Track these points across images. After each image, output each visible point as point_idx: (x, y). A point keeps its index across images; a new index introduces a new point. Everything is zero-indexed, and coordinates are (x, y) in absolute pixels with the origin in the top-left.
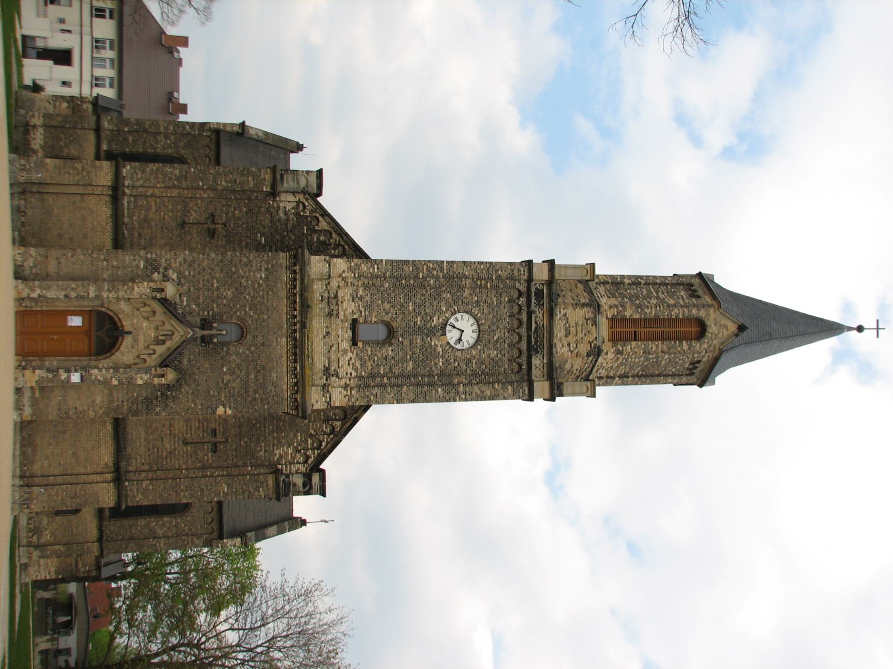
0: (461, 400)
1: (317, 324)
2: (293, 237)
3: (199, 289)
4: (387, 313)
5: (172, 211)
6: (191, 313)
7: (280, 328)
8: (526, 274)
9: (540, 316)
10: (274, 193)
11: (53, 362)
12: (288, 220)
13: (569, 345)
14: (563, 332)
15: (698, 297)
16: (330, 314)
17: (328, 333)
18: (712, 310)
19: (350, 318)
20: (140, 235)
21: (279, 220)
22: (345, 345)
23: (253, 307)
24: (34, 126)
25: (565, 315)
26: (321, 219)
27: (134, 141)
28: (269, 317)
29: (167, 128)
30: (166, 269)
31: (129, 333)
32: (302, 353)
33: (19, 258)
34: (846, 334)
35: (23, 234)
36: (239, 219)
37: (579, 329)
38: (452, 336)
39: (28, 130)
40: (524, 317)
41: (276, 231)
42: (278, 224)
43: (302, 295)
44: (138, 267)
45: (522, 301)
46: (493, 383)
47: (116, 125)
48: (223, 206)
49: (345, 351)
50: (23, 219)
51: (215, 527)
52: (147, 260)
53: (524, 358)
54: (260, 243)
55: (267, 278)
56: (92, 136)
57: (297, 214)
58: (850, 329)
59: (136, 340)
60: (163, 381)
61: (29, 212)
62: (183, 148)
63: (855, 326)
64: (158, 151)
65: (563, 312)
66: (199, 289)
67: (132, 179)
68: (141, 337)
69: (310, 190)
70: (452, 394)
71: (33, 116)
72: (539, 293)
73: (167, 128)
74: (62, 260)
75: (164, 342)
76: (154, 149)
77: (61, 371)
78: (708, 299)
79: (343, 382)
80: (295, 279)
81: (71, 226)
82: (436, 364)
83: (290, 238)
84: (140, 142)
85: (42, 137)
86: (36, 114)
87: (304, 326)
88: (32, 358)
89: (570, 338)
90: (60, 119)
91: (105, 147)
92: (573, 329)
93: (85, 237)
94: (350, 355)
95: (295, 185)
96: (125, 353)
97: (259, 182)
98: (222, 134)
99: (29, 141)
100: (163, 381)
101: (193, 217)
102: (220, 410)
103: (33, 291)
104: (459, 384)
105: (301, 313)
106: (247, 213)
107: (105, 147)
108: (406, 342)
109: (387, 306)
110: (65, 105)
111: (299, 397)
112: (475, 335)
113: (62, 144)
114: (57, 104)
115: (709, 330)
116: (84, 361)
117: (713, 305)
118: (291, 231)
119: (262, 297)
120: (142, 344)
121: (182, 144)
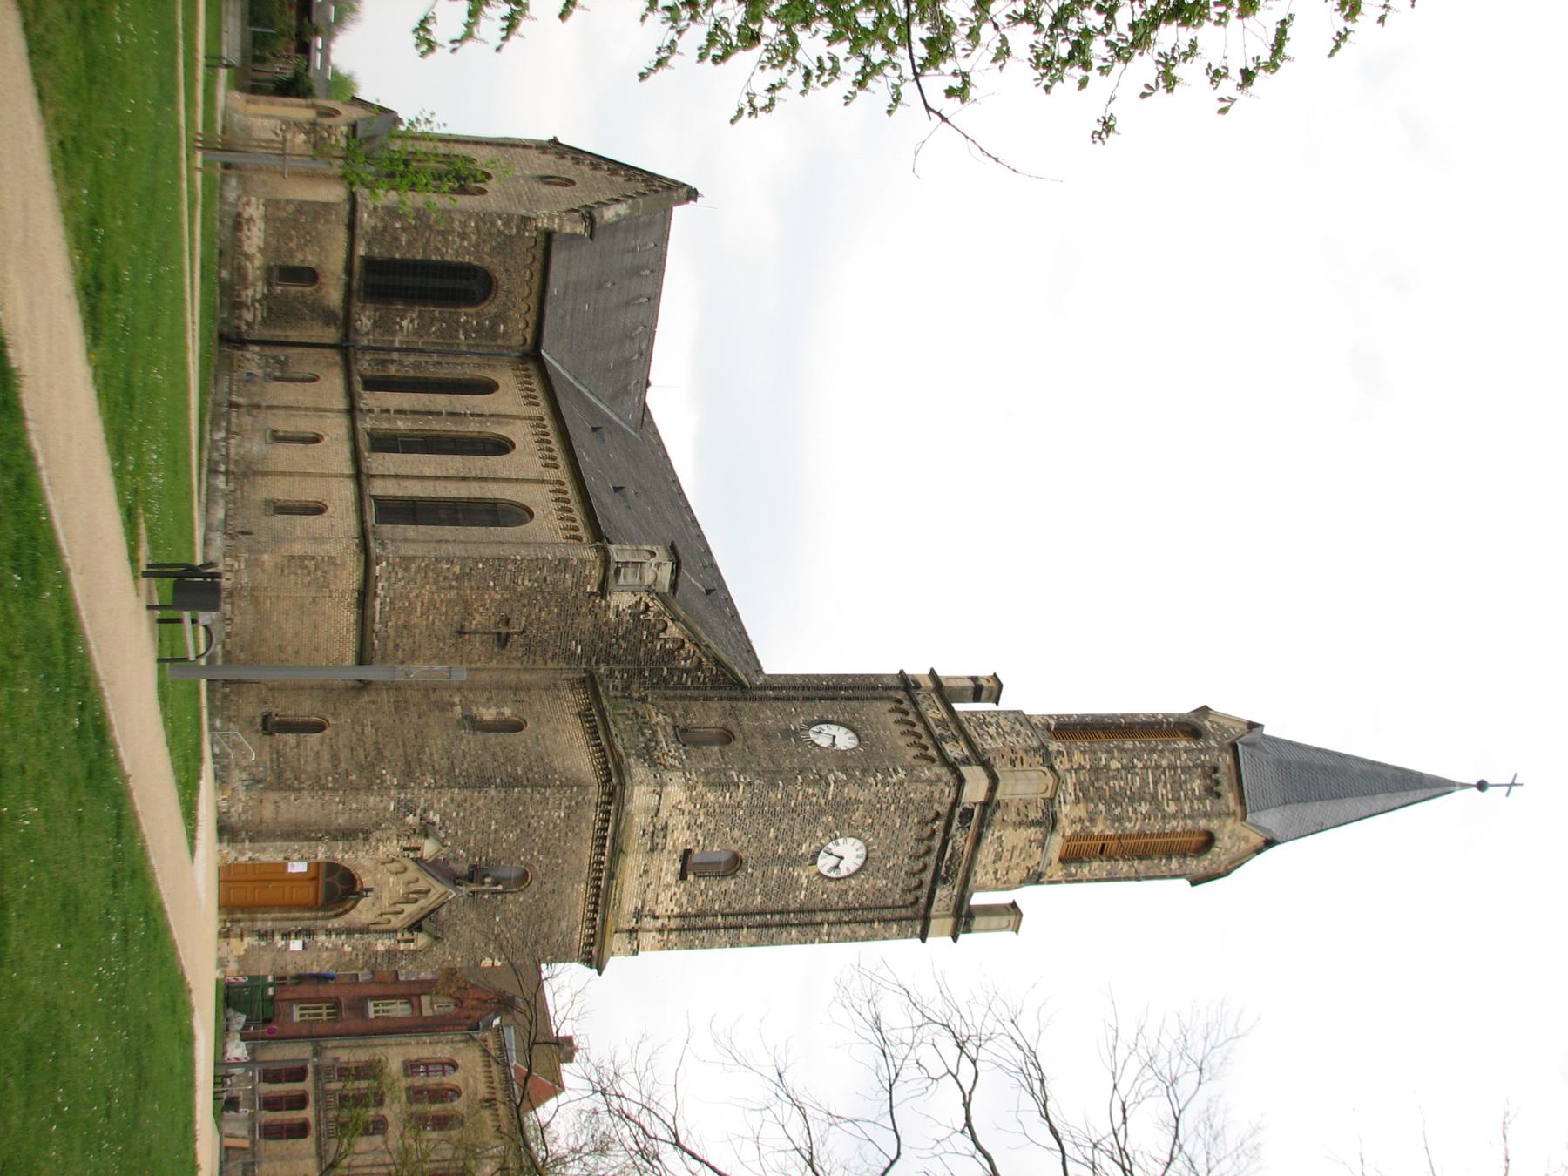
0: (821, 941)
1: (632, 864)
2: (624, 645)
3: (470, 833)
4: (736, 842)
5: (446, 614)
6: (455, 860)
7: (580, 872)
8: (953, 795)
9: (961, 840)
10: (603, 591)
11: (265, 922)
12: (620, 623)
13: (996, 872)
14: (991, 857)
15: (1218, 795)
16: (652, 850)
17: (646, 872)
18: (1230, 821)
19: (681, 849)
20: (396, 646)
21: (607, 623)
22: (671, 879)
23: (545, 850)
24: (251, 219)
25: (1000, 837)
26: (670, 623)
27: (409, 242)
28: (565, 861)
29: (465, 225)
30: (425, 811)
31: (370, 890)
32: (606, 904)
33: (225, 804)
34: (1457, 796)
35: (228, 647)
36: (546, 622)
37: (1017, 853)
38: (825, 863)
39: (240, 223)
40: (937, 843)
41: (601, 637)
42: (605, 629)
43: (614, 840)
44: (386, 809)
45: (939, 824)
46: (872, 921)
47: (382, 219)
48: (524, 606)
49: (668, 886)
50: (228, 629)
51: (528, 337)
52: (399, 801)
53: (925, 890)
54: (573, 654)
55: (568, 817)
56: (342, 235)
57: (635, 616)
58: (1465, 786)
59: (379, 898)
60: (412, 946)
61: (238, 619)
62: (490, 255)
63: (1475, 782)
64: (448, 258)
65: (997, 834)
66: (470, 833)
67: (388, 579)
68: (386, 894)
69: (658, 589)
70: (810, 936)
71: (248, 203)
72: (967, 814)
73: (465, 225)
74: (282, 804)
75: (416, 901)
76: (442, 255)
77: (278, 938)
78: (1231, 800)
79: (659, 923)
80: (607, 821)
81: (296, 635)
82: (795, 897)
83: (620, 647)
84: (419, 244)
85: (261, 234)
86: (254, 199)
87: (611, 876)
88: (239, 916)
89: (999, 865)
90: (291, 208)
91: (361, 251)
92: (1006, 854)
93: (316, 649)
94: (674, 889)
95: (637, 581)
96: (363, 912)
97: (581, 580)
98: (556, 236)
99: (240, 241)
100: (412, 946)
101: (477, 621)
102: (487, 962)
103: (242, 853)
104: (822, 924)
105: (611, 860)
106: (558, 615)
107: (361, 251)
108: (757, 874)
109: (737, 833)
110: (302, 137)
111: (594, 950)
112: (860, 861)
113: (293, 245)
114: (289, 136)
115: (1218, 844)
116: (306, 919)
117: (1234, 814)
118: (623, 637)
119: (559, 840)
120: (386, 902)
121: (487, 248)
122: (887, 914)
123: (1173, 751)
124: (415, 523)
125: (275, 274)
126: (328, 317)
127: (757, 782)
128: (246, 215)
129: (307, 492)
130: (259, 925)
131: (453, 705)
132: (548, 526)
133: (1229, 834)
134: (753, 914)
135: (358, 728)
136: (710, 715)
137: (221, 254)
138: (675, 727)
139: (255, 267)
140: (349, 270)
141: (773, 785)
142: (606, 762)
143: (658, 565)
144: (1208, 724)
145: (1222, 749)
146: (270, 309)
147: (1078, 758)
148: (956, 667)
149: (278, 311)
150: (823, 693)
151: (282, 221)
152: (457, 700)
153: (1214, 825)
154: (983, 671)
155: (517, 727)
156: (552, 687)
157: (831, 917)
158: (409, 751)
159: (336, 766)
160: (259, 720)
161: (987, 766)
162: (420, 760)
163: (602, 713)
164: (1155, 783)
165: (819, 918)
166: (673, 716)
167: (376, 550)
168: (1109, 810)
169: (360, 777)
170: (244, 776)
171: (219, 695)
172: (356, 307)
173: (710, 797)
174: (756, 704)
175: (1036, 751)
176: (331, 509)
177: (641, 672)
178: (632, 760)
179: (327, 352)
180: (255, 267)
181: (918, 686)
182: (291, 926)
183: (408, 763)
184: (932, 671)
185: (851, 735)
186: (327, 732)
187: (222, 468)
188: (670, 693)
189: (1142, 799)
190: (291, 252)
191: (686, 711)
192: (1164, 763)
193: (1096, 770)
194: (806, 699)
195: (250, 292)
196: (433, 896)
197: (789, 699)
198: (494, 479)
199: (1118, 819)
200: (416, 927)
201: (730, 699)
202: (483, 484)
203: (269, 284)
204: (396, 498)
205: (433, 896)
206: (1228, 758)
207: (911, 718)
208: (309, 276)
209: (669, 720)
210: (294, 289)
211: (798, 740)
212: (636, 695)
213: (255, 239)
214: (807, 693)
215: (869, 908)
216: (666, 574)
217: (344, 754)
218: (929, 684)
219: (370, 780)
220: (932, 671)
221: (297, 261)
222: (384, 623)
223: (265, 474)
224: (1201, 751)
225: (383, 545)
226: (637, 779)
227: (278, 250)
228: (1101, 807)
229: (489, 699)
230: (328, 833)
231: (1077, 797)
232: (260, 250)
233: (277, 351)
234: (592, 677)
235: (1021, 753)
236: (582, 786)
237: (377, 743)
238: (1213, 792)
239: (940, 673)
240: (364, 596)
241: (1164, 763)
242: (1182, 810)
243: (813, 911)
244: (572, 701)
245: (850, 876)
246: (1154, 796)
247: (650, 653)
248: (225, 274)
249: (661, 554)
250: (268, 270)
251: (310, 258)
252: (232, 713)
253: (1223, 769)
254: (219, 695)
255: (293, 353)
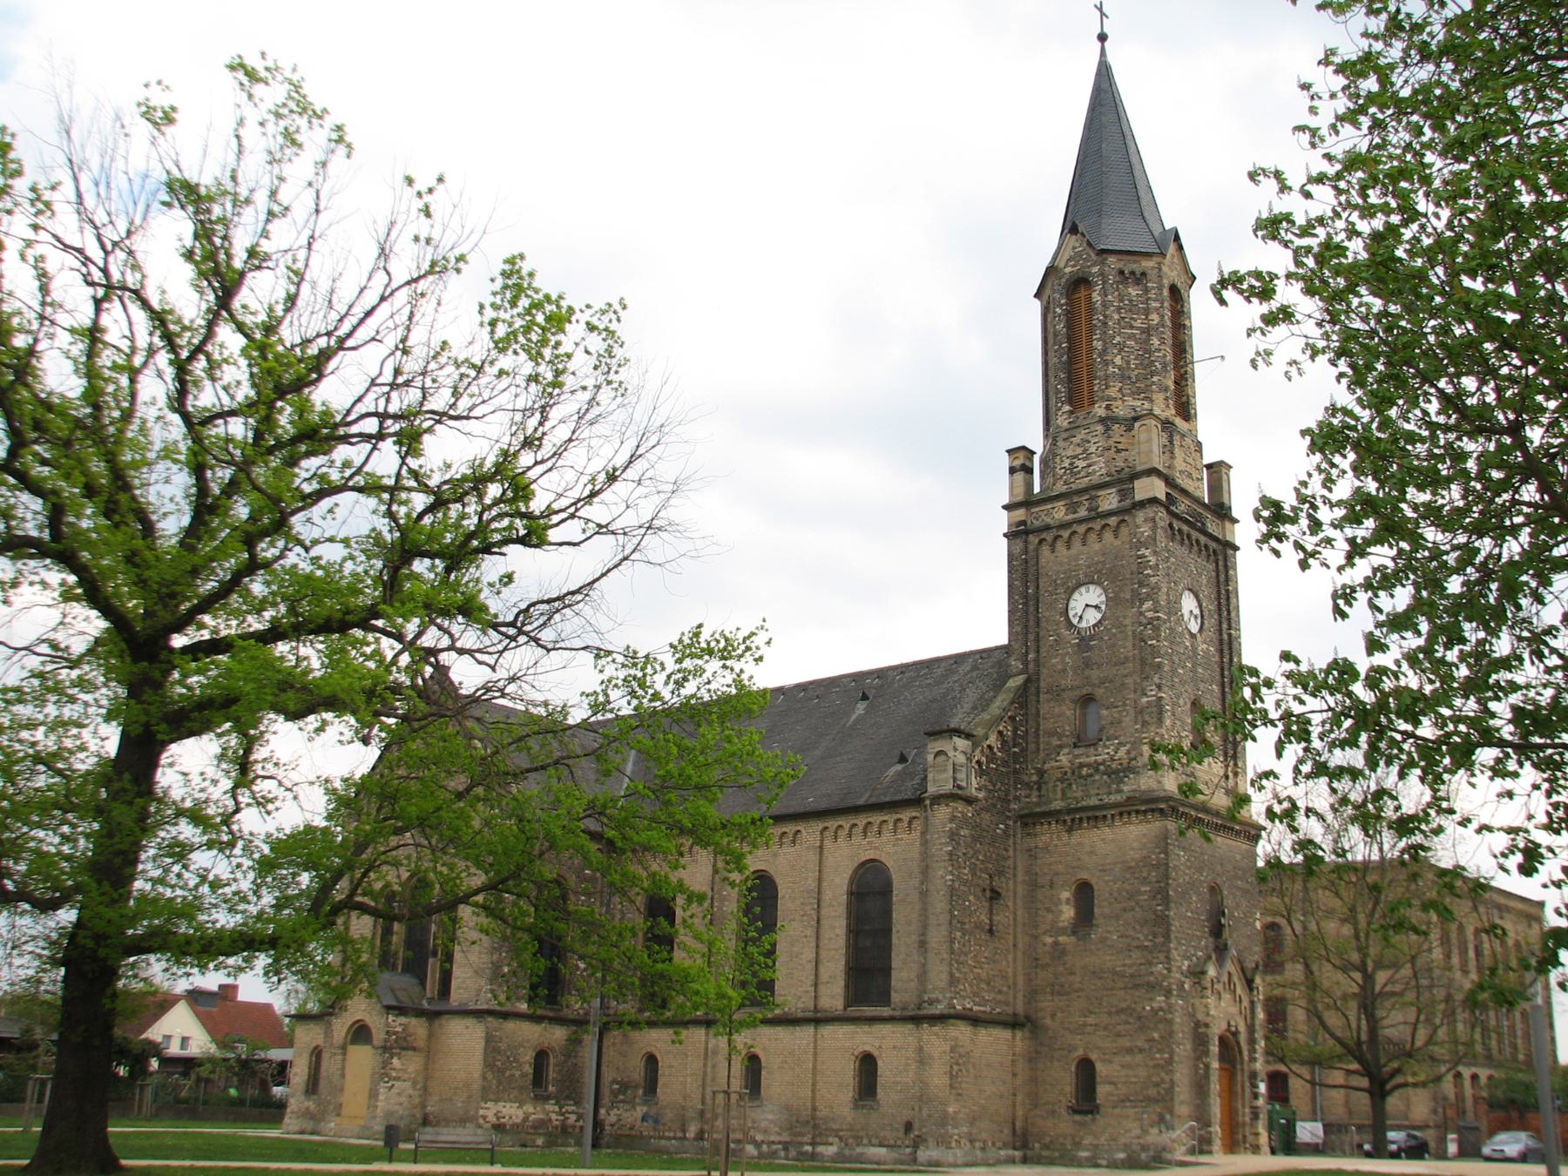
20: (1000, 992)
34: (1110, 59)
56: (510, 1025)
58: (1103, 53)
61: (984, 1135)
78: (1148, 264)
86: (481, 1112)
90: (490, 1076)
91: (523, 1007)
97: (965, 821)
107: (523, 1007)
110: (395, 1061)
122: (1222, 577)
123: (1105, 305)
124: (887, 971)
125: (540, 1092)
126: (575, 1041)
127: (1156, 680)
128: (494, 1120)
129: (847, 1072)
130: (1247, 1119)
131: (1056, 943)
132: (893, 845)
133: (1171, 274)
134: (1223, 693)
135: (1090, 1029)
136: (1059, 715)
137: (524, 1145)
138: (1075, 746)
139: (533, 1111)
140: (538, 1019)
141: (1159, 666)
142: (1137, 812)
143: (955, 749)
144: (1068, 270)
145: (1103, 263)
146: (568, 1098)
147: (1113, 392)
148: (1000, 489)
149: (570, 1091)
150: (1031, 609)
151: (500, 1083)
152: (1049, 940)
153: (1166, 282)
154: (1005, 462)
155: (1084, 893)
156: (1032, 854)
157: (1225, 626)
158: (1120, 985)
159: (1141, 1050)
160: (1078, 1118)
161: (1135, 476)
162: (1132, 976)
163: (1070, 811)
164: (1132, 327)
165: (1225, 637)
166: (1061, 747)
167: (939, 1008)
168: (1158, 374)
169: (1155, 1029)
170: (1155, 1131)
171: (1045, 1153)
172: (566, 1013)
173: (1168, 722)
174: (1044, 671)
175: (1108, 429)
176: (868, 1048)
177: (1016, 772)
178: (1125, 788)
179: (606, 1043)
180: (533, 1111)
181: (1023, 523)
182: (1248, 1090)
183: (1136, 986)
184: (1005, 507)
185: (1083, 589)
186: (1093, 1056)
187: (809, 1148)
188: (1032, 747)
189: (1147, 341)
190: (523, 1075)
191: (1053, 733)
192: (1116, 317)
193: (1123, 378)
194: (1038, 625)
195: (554, 1117)
196: (1233, 970)
197: (1037, 640)
198: (819, 893)
199: (1165, 366)
200: (1249, 983)
201: (1038, 693)
202: (823, 904)
203: (547, 1098)
204: (847, 987)
205: (1233, 970)
206: (1111, 259)
207: (1066, 534)
208: (541, 1057)
209: (1066, 750)
210: (552, 1073)
211: (1092, 638)
212: (1035, 778)
213: (512, 1112)
214: (1031, 623)
215: (1219, 592)
216: (961, 743)
217: (1125, 1042)
218: (1020, 514)
219: (1161, 1019)
220: (1005, 507)
221: (529, 1069)
222: (984, 1002)
223: (814, 1109)
224: (1104, 283)
225: (931, 1002)
226: (1154, 785)
227: (521, 1088)
228: (1155, 379)
229: (1049, 910)
230: (1198, 1059)
231: (1145, 398)
232: (520, 1107)
233: (606, 1092)
234: (1021, 817)
235: (1111, 442)
236: (1165, 836)
237: (1110, 1014)
238: (1140, 278)
239: (1006, 501)
240: (975, 1021)
241: (1116, 317)
242: (1157, 309)
243: (1221, 641)
244: (1049, 836)
245: (1200, 606)
246: (1143, 331)
247: (1005, 763)
248: (540, 1142)
249: (935, 746)
250: (537, 1098)
251: (528, 1056)
252: (1068, 1142)
253: (1121, 265)
254: (1045, 1153)
255: (608, 1075)
